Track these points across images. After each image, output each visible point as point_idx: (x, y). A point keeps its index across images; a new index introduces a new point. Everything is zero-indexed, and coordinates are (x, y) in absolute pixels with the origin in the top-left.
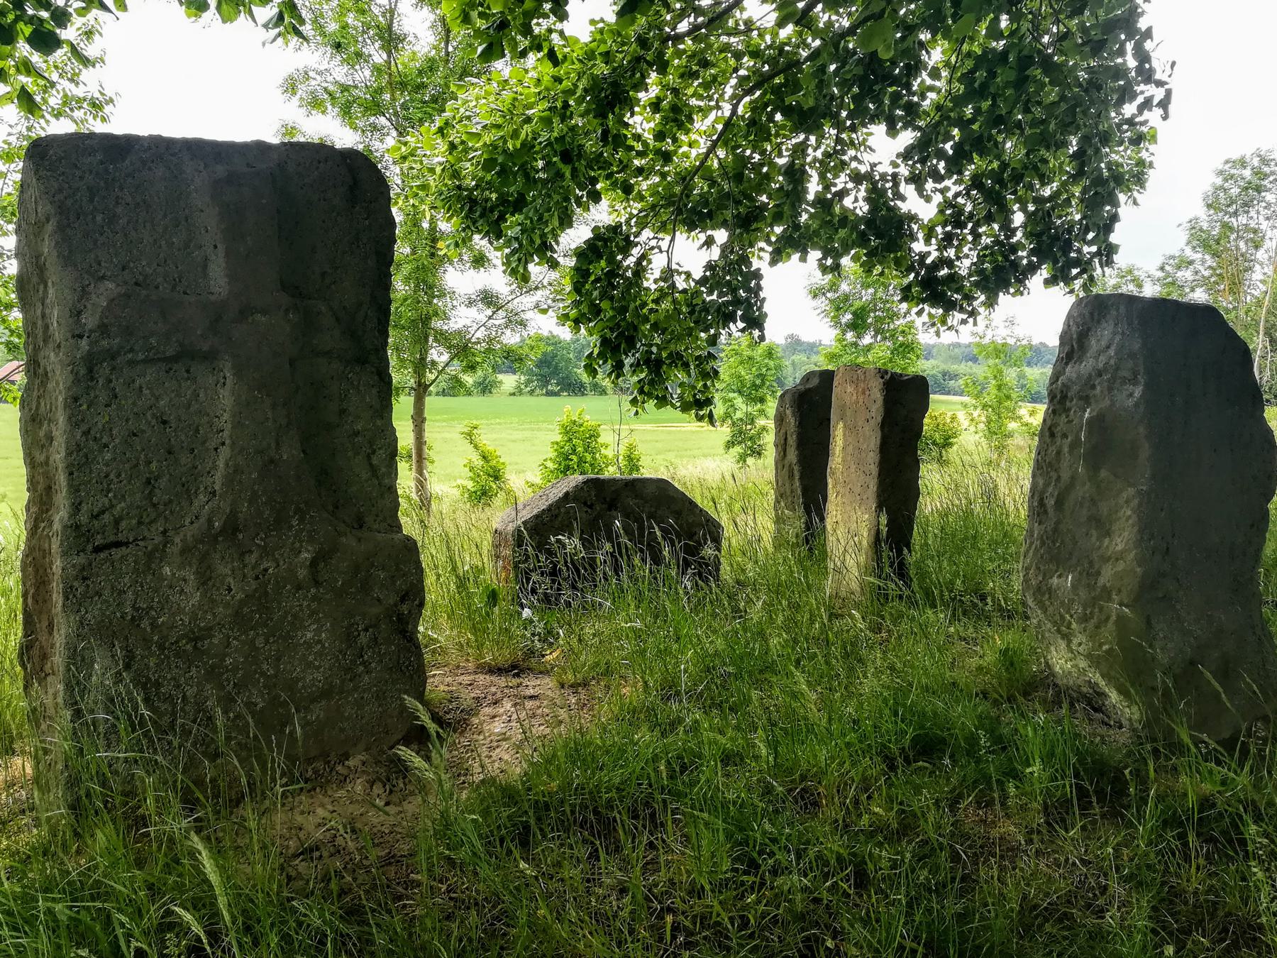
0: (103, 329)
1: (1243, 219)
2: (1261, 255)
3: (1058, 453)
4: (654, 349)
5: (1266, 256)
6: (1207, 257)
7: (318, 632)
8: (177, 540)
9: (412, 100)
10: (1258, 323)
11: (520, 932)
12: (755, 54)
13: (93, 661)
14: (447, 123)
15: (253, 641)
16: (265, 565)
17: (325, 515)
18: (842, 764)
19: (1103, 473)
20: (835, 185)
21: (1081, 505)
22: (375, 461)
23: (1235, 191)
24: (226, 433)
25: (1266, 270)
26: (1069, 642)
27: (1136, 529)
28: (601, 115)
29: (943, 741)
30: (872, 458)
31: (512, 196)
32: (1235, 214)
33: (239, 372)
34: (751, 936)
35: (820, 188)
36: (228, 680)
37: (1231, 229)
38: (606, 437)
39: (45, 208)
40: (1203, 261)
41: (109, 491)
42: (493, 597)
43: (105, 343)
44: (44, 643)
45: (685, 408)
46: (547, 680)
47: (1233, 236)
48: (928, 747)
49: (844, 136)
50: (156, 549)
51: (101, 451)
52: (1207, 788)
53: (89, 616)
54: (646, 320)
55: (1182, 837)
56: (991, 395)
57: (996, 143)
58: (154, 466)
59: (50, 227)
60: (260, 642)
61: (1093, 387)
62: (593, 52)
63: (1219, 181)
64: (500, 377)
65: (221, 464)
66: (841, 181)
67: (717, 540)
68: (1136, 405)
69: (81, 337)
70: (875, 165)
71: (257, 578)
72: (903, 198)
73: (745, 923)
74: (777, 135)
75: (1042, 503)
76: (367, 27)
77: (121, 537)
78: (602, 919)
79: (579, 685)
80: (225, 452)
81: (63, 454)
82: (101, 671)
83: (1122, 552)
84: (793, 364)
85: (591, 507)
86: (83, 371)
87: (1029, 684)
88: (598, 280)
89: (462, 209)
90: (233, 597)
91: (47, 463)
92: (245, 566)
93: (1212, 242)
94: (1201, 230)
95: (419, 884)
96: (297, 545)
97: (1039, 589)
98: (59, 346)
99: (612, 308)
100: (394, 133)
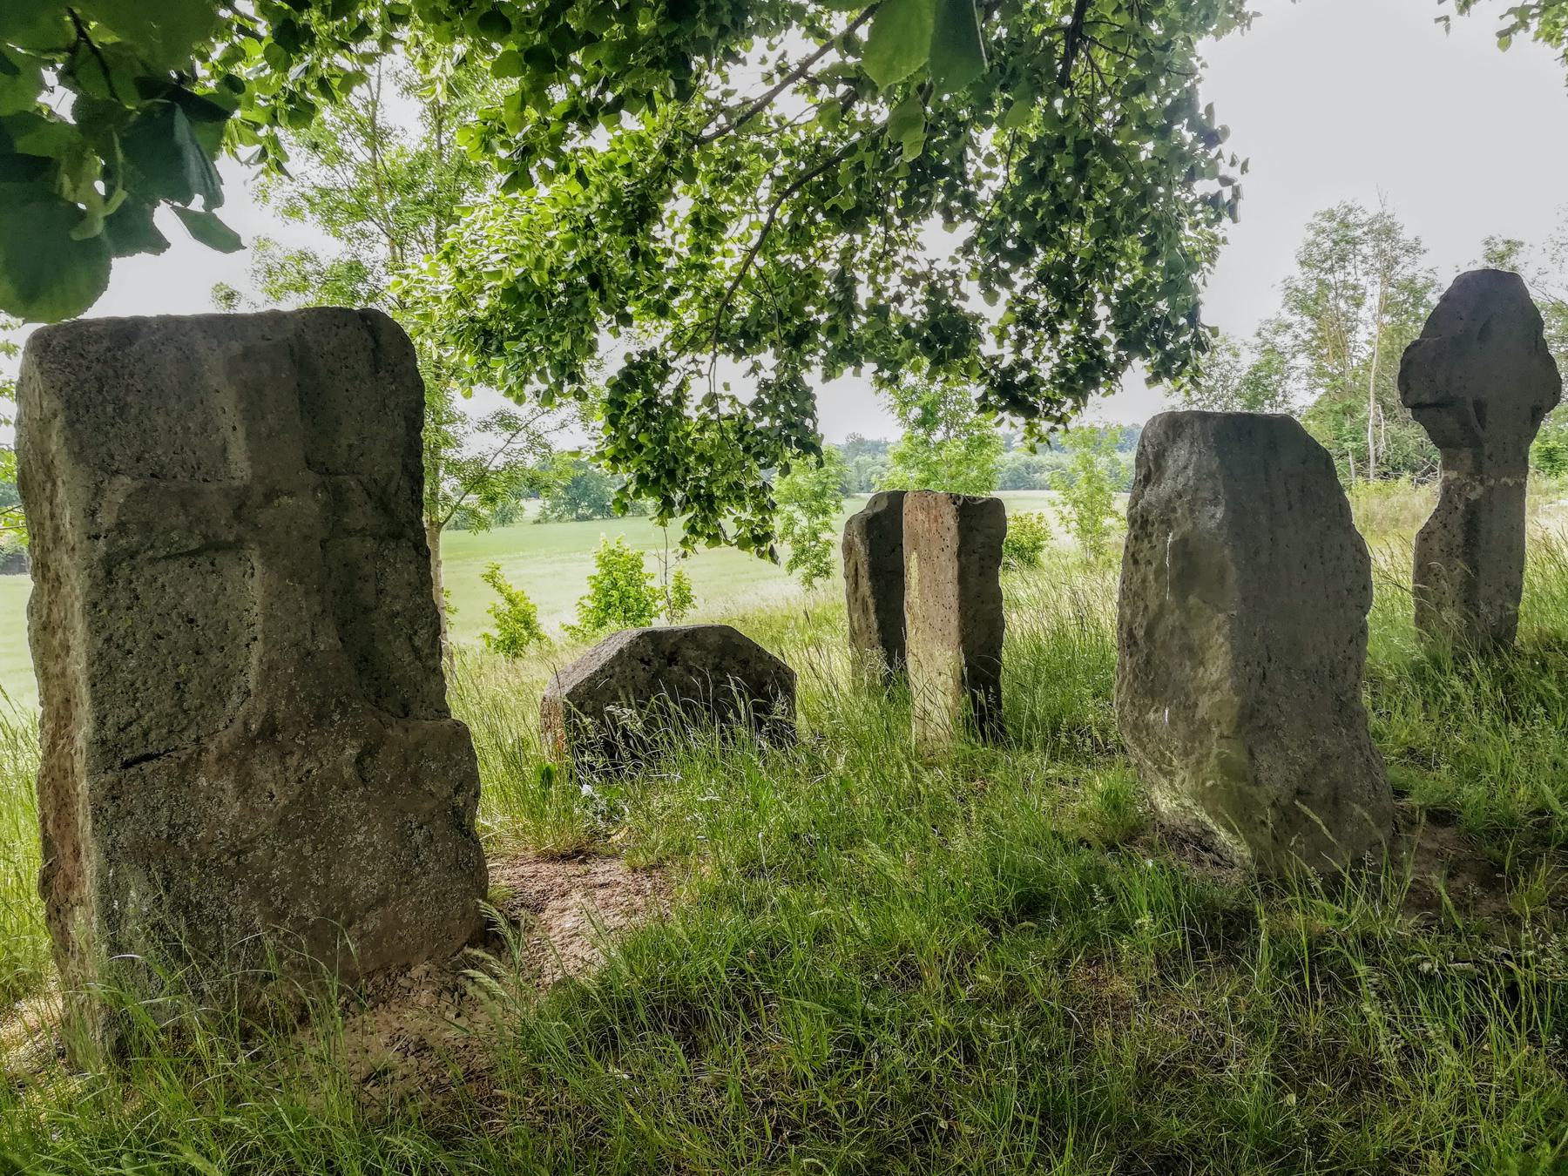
0: (121, 528)
1: (1340, 275)
2: (1363, 313)
3: (1144, 581)
4: (703, 483)
5: (1369, 315)
6: (1306, 319)
7: (369, 833)
8: (212, 747)
9: (404, 203)
10: (1368, 388)
11: (618, 1140)
12: (790, 152)
13: (128, 888)
14: (453, 248)
15: (300, 850)
16: (308, 766)
17: (368, 706)
18: (941, 931)
19: (1192, 600)
20: (887, 289)
21: (1172, 633)
22: (417, 642)
23: (1328, 245)
24: (258, 627)
25: (1371, 329)
26: (1171, 781)
27: (1229, 657)
28: (630, 231)
29: (1046, 897)
30: (951, 591)
31: (537, 321)
32: (1331, 270)
33: (268, 559)
34: (860, 1124)
35: (870, 294)
36: (274, 894)
37: (1329, 287)
38: (650, 565)
39: (51, 403)
40: (1303, 324)
41: (136, 700)
42: (547, 776)
43: (122, 542)
44: (69, 872)
45: (743, 544)
46: (616, 864)
47: (1332, 295)
48: (1032, 905)
49: (892, 233)
50: (190, 757)
51: (124, 658)
52: (1321, 924)
53: (121, 838)
54: (690, 451)
55: (1299, 978)
56: (1081, 490)
57: (1061, 234)
58: (182, 668)
59: (58, 423)
60: (307, 850)
61: (1174, 510)
62: (612, 163)
63: (1310, 236)
64: (523, 502)
65: (254, 661)
66: (894, 284)
67: (789, 691)
68: (1219, 527)
69: (97, 537)
70: (932, 262)
71: (300, 781)
72: (964, 297)
73: (853, 1110)
74: (821, 238)
75: (1131, 634)
76: (348, 121)
77: (150, 750)
78: (704, 1120)
79: (653, 867)
80: (257, 648)
81: (83, 665)
82: (137, 900)
83: (1218, 681)
84: (858, 466)
85: (648, 663)
86: (101, 574)
87: (1133, 828)
88: (633, 412)
89: (476, 342)
90: (276, 804)
91: (63, 674)
92: (286, 769)
93: (1310, 303)
94: (1297, 290)
95: (504, 1100)
96: (341, 742)
97: (1135, 726)
98: (73, 549)
99: (651, 440)
100: (385, 240)
